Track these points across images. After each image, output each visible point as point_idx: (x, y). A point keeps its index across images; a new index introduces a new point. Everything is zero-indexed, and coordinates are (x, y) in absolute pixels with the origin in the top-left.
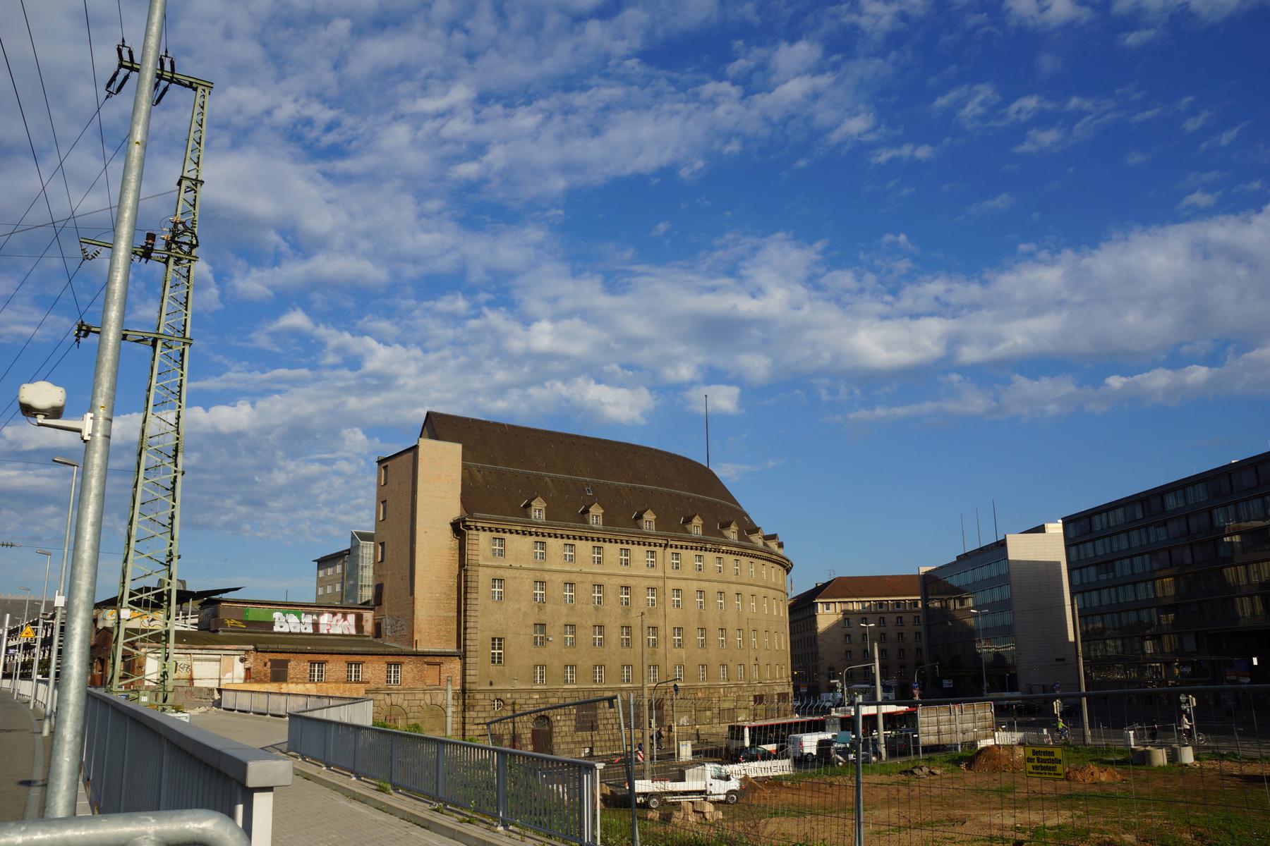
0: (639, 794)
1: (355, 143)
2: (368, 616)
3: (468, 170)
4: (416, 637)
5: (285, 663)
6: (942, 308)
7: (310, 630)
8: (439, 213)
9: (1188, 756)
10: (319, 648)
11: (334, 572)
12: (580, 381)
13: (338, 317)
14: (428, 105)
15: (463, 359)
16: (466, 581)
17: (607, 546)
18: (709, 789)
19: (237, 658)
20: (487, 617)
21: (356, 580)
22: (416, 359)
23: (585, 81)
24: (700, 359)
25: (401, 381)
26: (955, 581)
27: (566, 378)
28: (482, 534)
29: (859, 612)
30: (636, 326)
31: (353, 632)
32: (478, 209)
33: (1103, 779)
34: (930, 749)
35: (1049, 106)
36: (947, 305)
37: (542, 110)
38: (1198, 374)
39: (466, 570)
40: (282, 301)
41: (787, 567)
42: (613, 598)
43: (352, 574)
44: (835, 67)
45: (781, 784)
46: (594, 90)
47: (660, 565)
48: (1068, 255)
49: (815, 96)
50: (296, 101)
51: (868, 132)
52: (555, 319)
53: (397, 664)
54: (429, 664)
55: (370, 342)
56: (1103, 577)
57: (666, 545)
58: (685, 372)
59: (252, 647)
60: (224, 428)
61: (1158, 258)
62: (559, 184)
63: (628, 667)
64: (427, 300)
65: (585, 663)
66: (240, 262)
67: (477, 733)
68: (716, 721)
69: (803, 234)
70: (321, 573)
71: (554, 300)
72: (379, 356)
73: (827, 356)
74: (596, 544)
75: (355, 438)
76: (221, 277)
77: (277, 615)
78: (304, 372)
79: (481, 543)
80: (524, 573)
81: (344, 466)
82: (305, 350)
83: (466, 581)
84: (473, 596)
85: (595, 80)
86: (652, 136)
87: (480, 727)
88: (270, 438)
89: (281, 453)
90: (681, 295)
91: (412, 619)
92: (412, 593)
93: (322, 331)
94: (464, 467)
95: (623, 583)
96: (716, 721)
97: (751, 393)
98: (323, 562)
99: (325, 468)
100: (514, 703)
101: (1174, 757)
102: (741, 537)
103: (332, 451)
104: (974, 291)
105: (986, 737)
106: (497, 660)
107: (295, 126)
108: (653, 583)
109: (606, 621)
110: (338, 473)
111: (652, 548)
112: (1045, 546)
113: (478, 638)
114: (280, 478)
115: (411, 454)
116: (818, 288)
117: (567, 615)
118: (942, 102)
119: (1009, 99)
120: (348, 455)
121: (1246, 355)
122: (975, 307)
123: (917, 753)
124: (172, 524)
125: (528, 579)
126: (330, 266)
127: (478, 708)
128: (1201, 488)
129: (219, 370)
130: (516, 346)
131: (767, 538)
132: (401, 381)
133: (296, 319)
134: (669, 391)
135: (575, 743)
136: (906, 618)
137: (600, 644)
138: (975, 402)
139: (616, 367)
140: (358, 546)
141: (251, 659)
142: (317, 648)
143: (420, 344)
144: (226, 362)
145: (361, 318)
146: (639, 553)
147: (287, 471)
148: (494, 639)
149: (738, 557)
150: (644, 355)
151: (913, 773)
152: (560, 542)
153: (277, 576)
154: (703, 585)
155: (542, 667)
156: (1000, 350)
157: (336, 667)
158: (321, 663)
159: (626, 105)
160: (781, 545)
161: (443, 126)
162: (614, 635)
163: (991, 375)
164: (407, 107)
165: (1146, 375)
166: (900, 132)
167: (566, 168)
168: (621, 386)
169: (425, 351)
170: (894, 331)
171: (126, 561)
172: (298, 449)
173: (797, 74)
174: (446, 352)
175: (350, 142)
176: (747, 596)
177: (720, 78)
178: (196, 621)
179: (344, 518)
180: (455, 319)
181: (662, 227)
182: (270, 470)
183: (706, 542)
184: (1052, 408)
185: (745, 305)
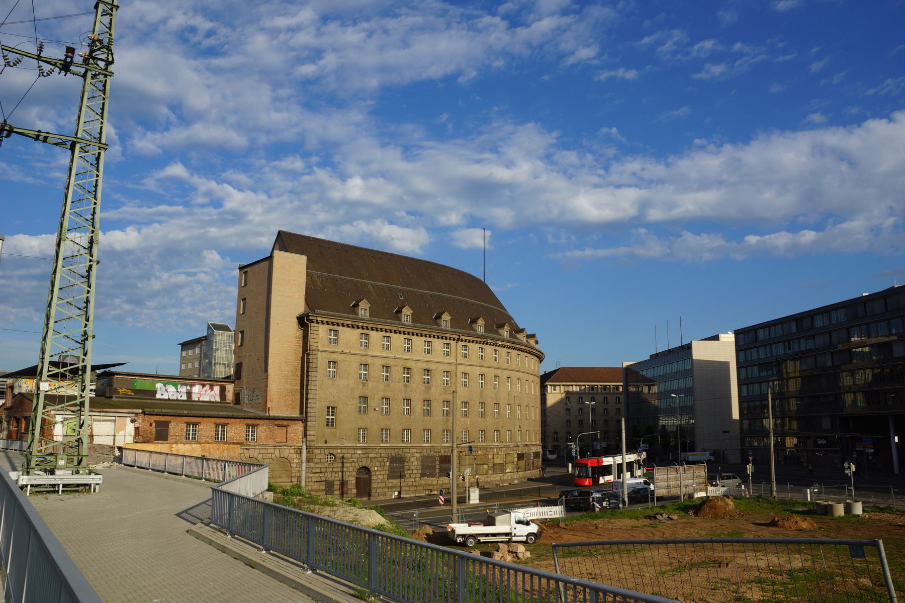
0: (459, 536)
1: (226, 47)
2: (230, 388)
3: (308, 70)
4: (269, 405)
5: (167, 424)
6: (639, 182)
7: (185, 398)
8: (289, 98)
9: (858, 509)
10: (194, 412)
11: (194, 352)
12: (378, 222)
13: (208, 170)
14: (282, 22)
15: (296, 203)
16: (308, 363)
17: (414, 338)
18: (514, 532)
19: (129, 419)
20: (323, 391)
21: (211, 359)
22: (262, 202)
23: (397, 11)
24: (466, 210)
25: (250, 217)
26: (648, 373)
27: (368, 219)
28: (321, 326)
29: (577, 393)
30: (422, 184)
31: (218, 399)
32: (316, 96)
33: (805, 527)
34: (660, 499)
35: (720, 48)
36: (641, 179)
37: (364, 30)
38: (808, 236)
39: (308, 354)
40: (168, 156)
41: (540, 357)
42: (418, 378)
43: (207, 356)
44: (576, 12)
45: (558, 526)
46: (403, 17)
47: (453, 354)
48: (728, 148)
49: (561, 30)
50: (185, 14)
51: (594, 58)
52: (365, 177)
53: (254, 426)
54: (278, 426)
55: (229, 188)
56: (763, 374)
57: (458, 340)
58: (453, 218)
59: (140, 411)
60: (118, 247)
61: (788, 154)
62: (373, 83)
63: (428, 431)
64: (275, 160)
65: (396, 427)
66: (139, 128)
67: (315, 479)
68: (490, 472)
69: (547, 125)
70: (184, 354)
71: (364, 164)
72: (235, 199)
73: (555, 211)
74: (407, 336)
75: (213, 257)
76: (124, 137)
77: (159, 386)
78: (180, 208)
79: (320, 333)
80: (353, 358)
81: (202, 277)
82: (181, 192)
83: (308, 363)
84: (314, 374)
85: (404, 10)
86: (445, 49)
87: (317, 475)
88: (151, 255)
89: (157, 267)
90: (457, 163)
91: (266, 391)
92: (266, 370)
93: (195, 179)
94: (308, 274)
95: (425, 366)
96: (490, 472)
97: (499, 235)
98: (186, 345)
99: (190, 279)
100: (343, 457)
101: (848, 509)
102: (511, 335)
103: (195, 267)
104: (657, 170)
105: (701, 490)
106: (331, 423)
107: (183, 31)
108: (448, 368)
109: (412, 396)
110: (197, 282)
111: (448, 341)
112: (723, 350)
113: (317, 406)
114: (156, 285)
115: (267, 263)
116: (552, 163)
117: (384, 391)
118: (647, 40)
119: (695, 40)
120: (206, 270)
121: (838, 226)
122: (661, 182)
123: (653, 501)
124: (86, 307)
125: (355, 362)
126: (204, 132)
127: (316, 460)
128: (842, 311)
129: (117, 205)
130: (336, 195)
131: (529, 336)
132: (250, 217)
133: (177, 170)
134: (440, 232)
135: (388, 488)
136: (610, 398)
137: (408, 413)
138: (655, 248)
139: (403, 213)
140: (213, 334)
141: (140, 421)
142: (191, 411)
143: (266, 192)
144: (123, 199)
145: (224, 171)
146: (438, 344)
147: (163, 279)
148: (328, 408)
149: (509, 350)
150: (426, 206)
151: (656, 518)
152: (380, 334)
153: (150, 354)
154: (484, 370)
155: (364, 430)
156: (676, 213)
157: (206, 428)
158: (195, 424)
159: (422, 29)
160: (537, 342)
161: (292, 37)
162: (418, 406)
163: (668, 230)
164: (267, 23)
165: (773, 236)
166: (618, 60)
167: (383, 69)
168: (407, 227)
169: (270, 197)
170: (603, 196)
171: (44, 339)
172: (172, 264)
173: (551, 14)
174: (285, 198)
175: (223, 46)
176: (515, 379)
177: (494, 14)
178: (94, 387)
179: (201, 314)
180: (293, 175)
181: (445, 117)
182: (149, 279)
183: (488, 338)
184: (707, 256)
185: (501, 173)
